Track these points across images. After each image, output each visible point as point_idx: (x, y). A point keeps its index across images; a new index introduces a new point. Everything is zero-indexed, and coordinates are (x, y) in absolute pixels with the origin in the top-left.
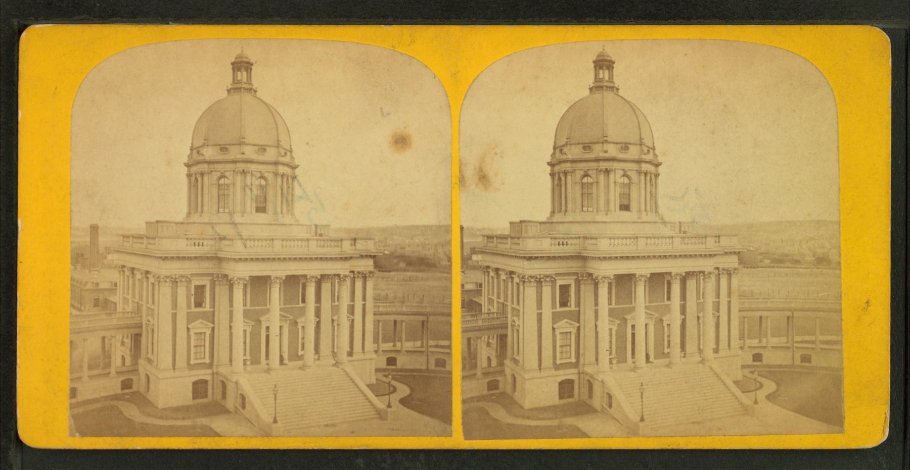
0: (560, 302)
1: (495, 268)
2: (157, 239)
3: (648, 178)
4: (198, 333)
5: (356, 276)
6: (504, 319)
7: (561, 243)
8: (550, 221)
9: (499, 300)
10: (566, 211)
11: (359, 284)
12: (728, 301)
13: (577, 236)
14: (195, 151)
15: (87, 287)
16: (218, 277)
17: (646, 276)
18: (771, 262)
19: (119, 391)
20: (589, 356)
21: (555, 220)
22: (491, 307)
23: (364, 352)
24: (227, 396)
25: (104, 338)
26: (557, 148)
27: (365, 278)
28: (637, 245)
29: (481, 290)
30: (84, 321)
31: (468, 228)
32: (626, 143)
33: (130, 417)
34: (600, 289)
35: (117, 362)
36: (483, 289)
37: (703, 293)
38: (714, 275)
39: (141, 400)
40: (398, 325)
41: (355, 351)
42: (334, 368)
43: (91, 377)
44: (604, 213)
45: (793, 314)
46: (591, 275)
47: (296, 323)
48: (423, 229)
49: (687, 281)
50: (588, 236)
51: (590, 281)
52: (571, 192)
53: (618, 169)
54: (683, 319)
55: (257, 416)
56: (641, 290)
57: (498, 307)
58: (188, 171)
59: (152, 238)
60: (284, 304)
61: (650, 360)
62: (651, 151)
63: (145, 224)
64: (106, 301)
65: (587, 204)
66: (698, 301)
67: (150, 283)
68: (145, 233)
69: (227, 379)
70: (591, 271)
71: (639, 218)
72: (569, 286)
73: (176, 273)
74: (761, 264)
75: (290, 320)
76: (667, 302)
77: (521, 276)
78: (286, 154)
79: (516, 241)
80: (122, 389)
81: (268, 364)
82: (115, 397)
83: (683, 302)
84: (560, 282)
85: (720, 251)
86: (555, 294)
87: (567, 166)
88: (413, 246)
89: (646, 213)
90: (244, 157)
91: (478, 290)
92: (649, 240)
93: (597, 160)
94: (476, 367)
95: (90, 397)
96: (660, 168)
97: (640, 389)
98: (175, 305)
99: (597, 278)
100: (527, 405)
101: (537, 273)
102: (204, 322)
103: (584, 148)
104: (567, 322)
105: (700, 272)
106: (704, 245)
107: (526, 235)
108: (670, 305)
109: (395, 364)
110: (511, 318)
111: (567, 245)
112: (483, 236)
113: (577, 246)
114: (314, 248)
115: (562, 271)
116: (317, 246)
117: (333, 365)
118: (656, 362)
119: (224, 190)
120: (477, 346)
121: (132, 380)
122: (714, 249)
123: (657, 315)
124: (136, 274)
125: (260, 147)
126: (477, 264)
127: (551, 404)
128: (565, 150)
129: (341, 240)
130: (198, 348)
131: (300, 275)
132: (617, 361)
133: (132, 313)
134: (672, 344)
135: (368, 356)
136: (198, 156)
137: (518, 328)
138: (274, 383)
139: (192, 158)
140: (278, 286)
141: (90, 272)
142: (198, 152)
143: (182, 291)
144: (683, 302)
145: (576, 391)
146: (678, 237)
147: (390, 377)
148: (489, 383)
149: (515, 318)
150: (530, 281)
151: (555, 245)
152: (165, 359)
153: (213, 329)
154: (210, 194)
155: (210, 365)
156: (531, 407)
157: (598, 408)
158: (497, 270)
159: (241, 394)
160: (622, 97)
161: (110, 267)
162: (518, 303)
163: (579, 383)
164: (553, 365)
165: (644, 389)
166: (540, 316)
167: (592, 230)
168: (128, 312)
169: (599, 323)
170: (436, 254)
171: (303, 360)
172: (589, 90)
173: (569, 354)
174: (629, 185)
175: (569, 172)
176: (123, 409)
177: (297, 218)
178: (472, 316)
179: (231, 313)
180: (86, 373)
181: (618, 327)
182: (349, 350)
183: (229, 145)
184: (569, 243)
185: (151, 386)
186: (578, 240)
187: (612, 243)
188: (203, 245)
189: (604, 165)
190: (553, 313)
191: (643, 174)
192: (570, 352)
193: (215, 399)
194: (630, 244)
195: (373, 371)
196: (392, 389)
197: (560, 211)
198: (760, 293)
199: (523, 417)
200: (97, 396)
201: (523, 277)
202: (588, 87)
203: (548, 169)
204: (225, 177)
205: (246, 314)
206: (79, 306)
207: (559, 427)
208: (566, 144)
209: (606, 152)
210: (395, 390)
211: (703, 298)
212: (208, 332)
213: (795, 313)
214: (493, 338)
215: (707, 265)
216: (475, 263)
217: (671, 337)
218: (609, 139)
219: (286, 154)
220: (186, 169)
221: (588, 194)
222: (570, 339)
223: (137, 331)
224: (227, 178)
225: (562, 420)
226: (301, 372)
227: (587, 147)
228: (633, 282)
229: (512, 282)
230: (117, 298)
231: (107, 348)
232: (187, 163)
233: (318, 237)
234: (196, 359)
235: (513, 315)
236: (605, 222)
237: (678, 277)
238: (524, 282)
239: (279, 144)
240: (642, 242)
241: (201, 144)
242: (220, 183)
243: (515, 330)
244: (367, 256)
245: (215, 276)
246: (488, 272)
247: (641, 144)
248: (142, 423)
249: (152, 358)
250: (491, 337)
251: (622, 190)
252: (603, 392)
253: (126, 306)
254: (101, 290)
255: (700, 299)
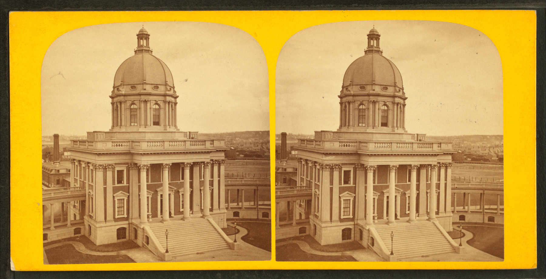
0: (117, 181)
1: (305, 159)
2: (94, 143)
3: (170, 105)
4: (119, 199)
5: (441, 165)
6: (84, 191)
7: (118, 145)
8: (339, 131)
9: (307, 179)
10: (349, 126)
11: (443, 171)
12: (218, 180)
13: (127, 141)
14: (116, 89)
15: (52, 173)
16: (131, 165)
17: (169, 165)
18: (244, 157)
19: (73, 235)
20: (135, 213)
21: (114, 131)
22: (76, 184)
23: (445, 212)
24: (363, 239)
25: (63, 204)
26: (116, 87)
27: (446, 168)
28: (164, 146)
29: (297, 173)
30: (51, 193)
31: (61, 135)
32: (157, 85)
33: (80, 251)
34: (368, 174)
35: (71, 218)
36: (298, 171)
37: (430, 178)
38: (437, 167)
39: (87, 241)
40: (466, 196)
41: (440, 211)
42: (427, 222)
43: (56, 227)
44: (372, 128)
45: (257, 188)
46: (136, 164)
47: (178, 192)
48: (482, 137)
49: (421, 170)
50: (362, 141)
51: (135, 168)
52: (124, 114)
53: (152, 100)
54: (191, 191)
55: (381, 250)
56: (393, 175)
57: (80, 184)
58: (112, 101)
59: (91, 142)
60: (171, 181)
61: (398, 218)
62: (172, 89)
63: (87, 133)
64: (64, 181)
65: (361, 121)
66: (427, 183)
67: (317, 169)
68: (87, 139)
69: (363, 228)
70: (136, 162)
71: (165, 130)
72: (350, 171)
73: (106, 163)
74: (237, 157)
75: (175, 190)
76: (408, 183)
77: (321, 165)
78: (170, 89)
79: (318, 143)
80: (75, 234)
81: (162, 217)
82: (70, 239)
83: (418, 183)
84: (117, 169)
85: (440, 152)
86: (341, 176)
87: (350, 99)
88: (478, 149)
89: (397, 128)
90: (374, 92)
91: (295, 173)
92: (398, 145)
93: (140, 95)
94: (292, 219)
95: (56, 239)
96: (406, 101)
97: (391, 235)
98: (105, 183)
99: (140, 166)
100: (323, 243)
101: (103, 163)
102: (349, 193)
103: (132, 87)
104: (348, 193)
105: (428, 165)
106: (431, 149)
107: (97, 140)
108: (183, 182)
109: (464, 220)
110: (88, 190)
111: (349, 146)
112: (71, 141)
113: (128, 147)
114: (189, 146)
115: (344, 162)
116: (191, 145)
117: (427, 220)
118: (401, 219)
119: (134, 112)
120: (293, 206)
121: (306, 228)
122: (438, 151)
123: (402, 191)
124: (82, 164)
125: (384, 86)
126: (294, 156)
127: (113, 242)
128: (349, 88)
129: (433, 144)
130: (120, 208)
131: (408, 165)
132: (152, 216)
133: (79, 188)
134: (185, 206)
135: (448, 214)
136: (347, 91)
137: (92, 197)
138: (392, 230)
139: (343, 93)
140: (167, 169)
141: (281, 162)
142: (118, 89)
143: (109, 174)
144: (418, 183)
145: (352, 235)
146: (415, 143)
147: (461, 227)
148: (75, 230)
149: (91, 191)
150: (100, 168)
151: (114, 146)
152: (100, 216)
153: (129, 196)
154: (125, 114)
155: (353, 220)
156: (101, 244)
157: (140, 245)
158: (79, 161)
159: (371, 237)
160: (154, 56)
161: (66, 160)
162: (92, 182)
163: (354, 231)
164: (339, 219)
165: (393, 235)
166: (105, 189)
167: (136, 137)
168: (78, 187)
169: (141, 193)
170: (489, 153)
171: (409, 216)
172: (134, 52)
173: (123, 212)
174: (387, 111)
175: (351, 102)
176: (75, 246)
177: (178, 128)
178: (64, 189)
179: (139, 187)
180: (53, 224)
181: (378, 197)
182: (437, 210)
183: (136, 84)
184: (123, 145)
185: (92, 232)
186: (129, 143)
187: (376, 146)
188: (122, 146)
189: (143, 98)
190: (340, 187)
191: (396, 104)
192: (350, 211)
193: (130, 239)
194: (160, 145)
195: (451, 223)
196: (462, 235)
197: (117, 125)
198: (238, 175)
199: (95, 250)
200: (60, 238)
201: (322, 165)
202: (134, 50)
203: (339, 100)
204: (363, 104)
205: (149, 187)
206: (48, 184)
207: (118, 256)
208: (350, 85)
209: (374, 90)
210: (464, 235)
211: (430, 181)
212: (126, 199)
213: (259, 187)
214: (303, 202)
215: (433, 161)
216: (293, 156)
217: (184, 202)
218: (147, 82)
219: (170, 89)
220: (110, 100)
221: (362, 115)
222: (124, 203)
223: (82, 199)
224: (364, 105)
225: (344, 252)
226: (408, 224)
227: (363, 87)
228: (388, 170)
229: (89, 169)
230: (71, 179)
231: (65, 210)
232: (112, 96)
233: (418, 142)
234: (344, 215)
235: (315, 188)
236: (373, 133)
237: (416, 168)
238: (96, 169)
239: (395, 84)
240: (167, 144)
241: (119, 84)
242: (131, 107)
243: (90, 198)
244: (447, 154)
245: (129, 164)
246: (74, 162)
247: (395, 86)
248: (87, 255)
249: (92, 215)
250: (76, 201)
251: (383, 114)
252: (369, 236)
253: (76, 184)
254: (288, 173)
255: (428, 182)
